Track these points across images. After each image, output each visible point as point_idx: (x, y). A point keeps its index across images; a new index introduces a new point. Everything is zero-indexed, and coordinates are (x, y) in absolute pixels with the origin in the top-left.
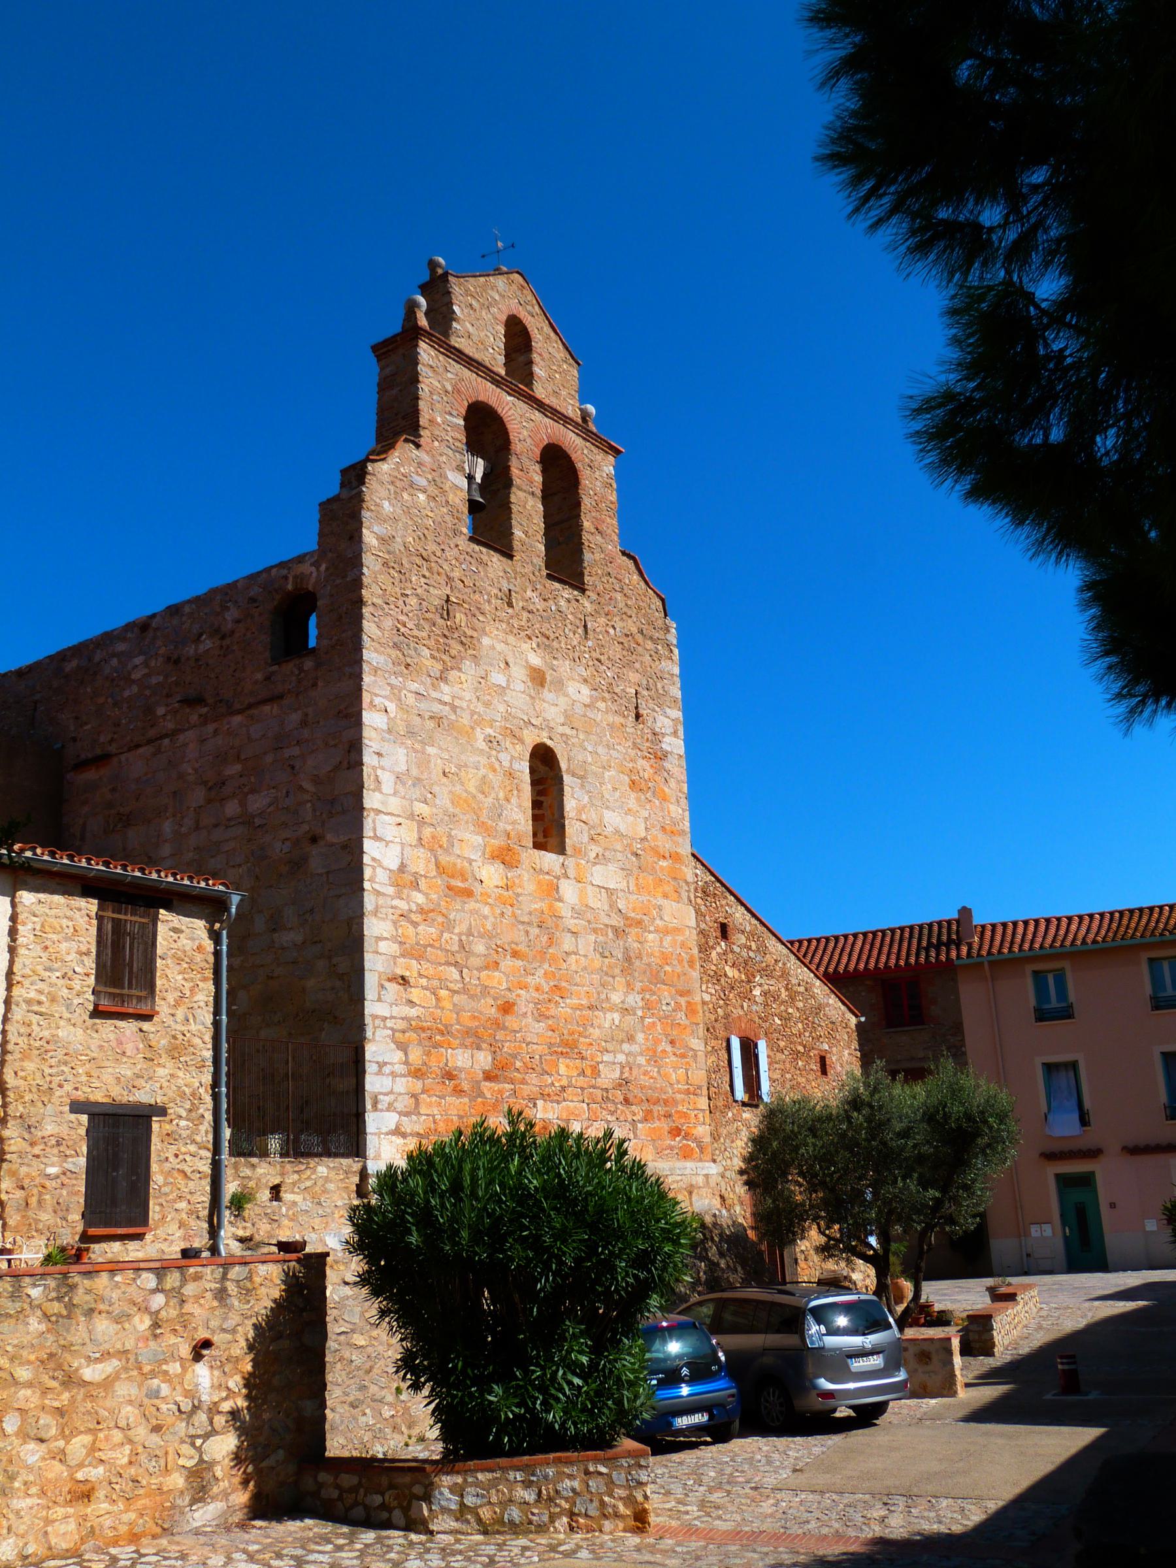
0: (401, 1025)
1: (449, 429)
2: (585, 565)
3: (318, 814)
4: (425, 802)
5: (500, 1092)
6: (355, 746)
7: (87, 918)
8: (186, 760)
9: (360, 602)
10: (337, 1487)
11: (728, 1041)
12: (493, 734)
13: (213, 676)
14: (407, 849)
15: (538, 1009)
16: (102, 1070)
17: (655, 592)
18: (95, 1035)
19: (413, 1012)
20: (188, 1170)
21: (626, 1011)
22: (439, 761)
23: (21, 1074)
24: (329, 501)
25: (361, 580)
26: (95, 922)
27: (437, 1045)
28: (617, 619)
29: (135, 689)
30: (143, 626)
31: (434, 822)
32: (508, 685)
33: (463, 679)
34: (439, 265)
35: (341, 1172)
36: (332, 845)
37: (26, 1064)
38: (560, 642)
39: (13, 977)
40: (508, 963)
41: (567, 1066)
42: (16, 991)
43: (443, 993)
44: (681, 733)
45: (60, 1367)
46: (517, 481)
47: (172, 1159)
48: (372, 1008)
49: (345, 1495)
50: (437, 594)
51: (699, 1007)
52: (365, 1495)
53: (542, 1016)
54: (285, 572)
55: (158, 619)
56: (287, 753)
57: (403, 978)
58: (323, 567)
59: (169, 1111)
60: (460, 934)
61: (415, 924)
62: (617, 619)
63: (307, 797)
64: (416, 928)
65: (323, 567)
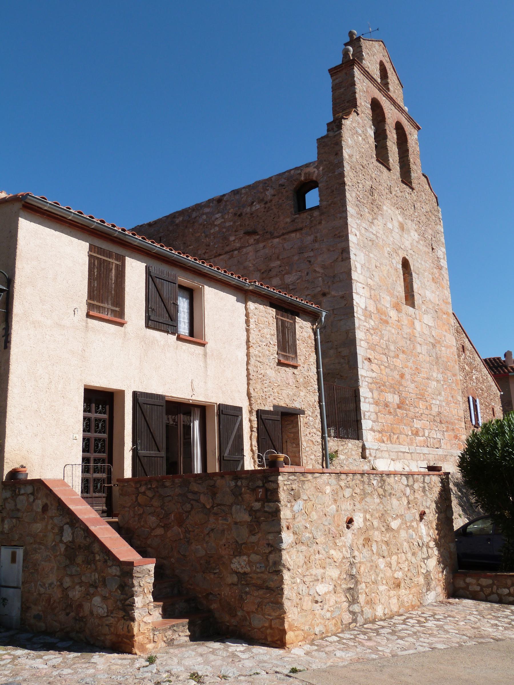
0: (370, 381)
1: (366, 109)
2: (412, 178)
3: (325, 282)
4: (371, 279)
5: (403, 414)
6: (345, 252)
7: (272, 318)
8: (248, 260)
9: (344, 184)
10: (479, 585)
11: (468, 398)
12: (390, 251)
13: (261, 221)
14: (367, 299)
15: (412, 378)
16: (282, 391)
17: (434, 194)
18: (278, 374)
19: (374, 375)
20: (314, 441)
21: (438, 381)
22: (374, 260)
23: (256, 390)
24: (322, 138)
25: (344, 173)
26: (275, 320)
27: (382, 391)
28: (423, 204)
29: (217, 229)
30: (219, 200)
31: (375, 288)
32: (393, 229)
33: (379, 224)
34: (354, 34)
35: (356, 446)
36: (334, 297)
37: (257, 385)
38: (407, 212)
39: (249, 343)
40: (401, 356)
41: (422, 404)
42: (251, 350)
43: (382, 367)
44: (446, 258)
45: (385, 521)
46: (389, 137)
47: (308, 435)
48: (361, 372)
49: (484, 589)
50: (369, 183)
51: (459, 382)
52: (497, 589)
53: (413, 381)
54: (299, 171)
55: (227, 196)
56: (306, 255)
57: (369, 359)
58: (321, 168)
59: (306, 412)
60: (386, 341)
61: (372, 335)
62: (423, 204)
63: (320, 275)
64: (372, 336)
65: (321, 168)
